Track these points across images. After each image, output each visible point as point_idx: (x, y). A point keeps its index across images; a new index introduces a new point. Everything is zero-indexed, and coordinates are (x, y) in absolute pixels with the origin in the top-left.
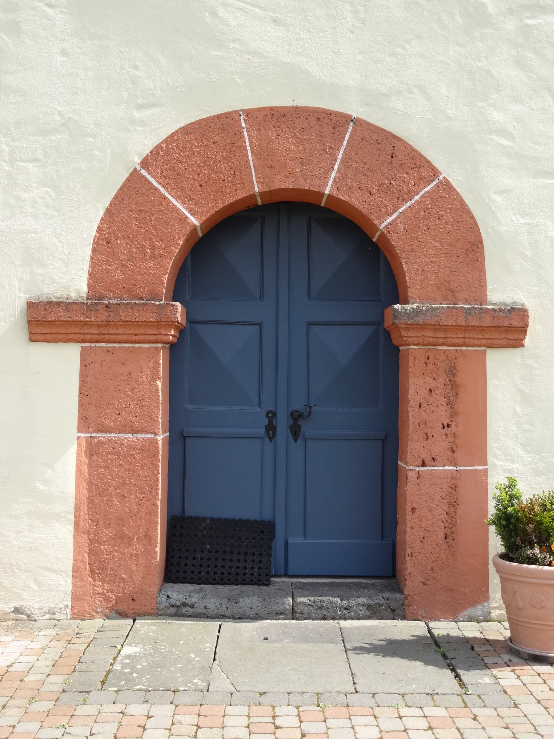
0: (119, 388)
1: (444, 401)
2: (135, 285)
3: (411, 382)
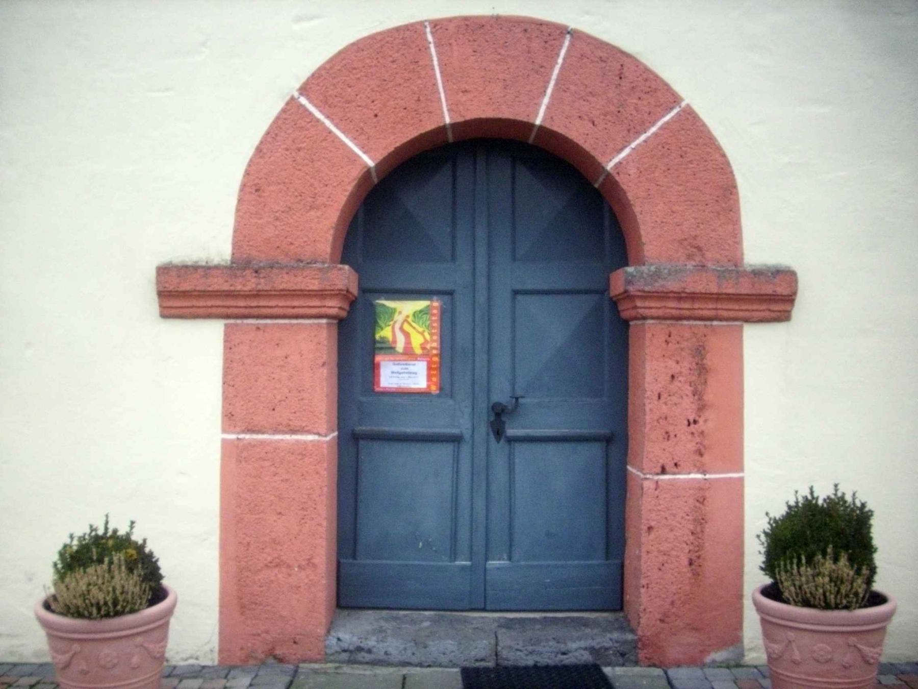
0: (273, 376)
1: (688, 389)
2: (292, 244)
3: (648, 366)
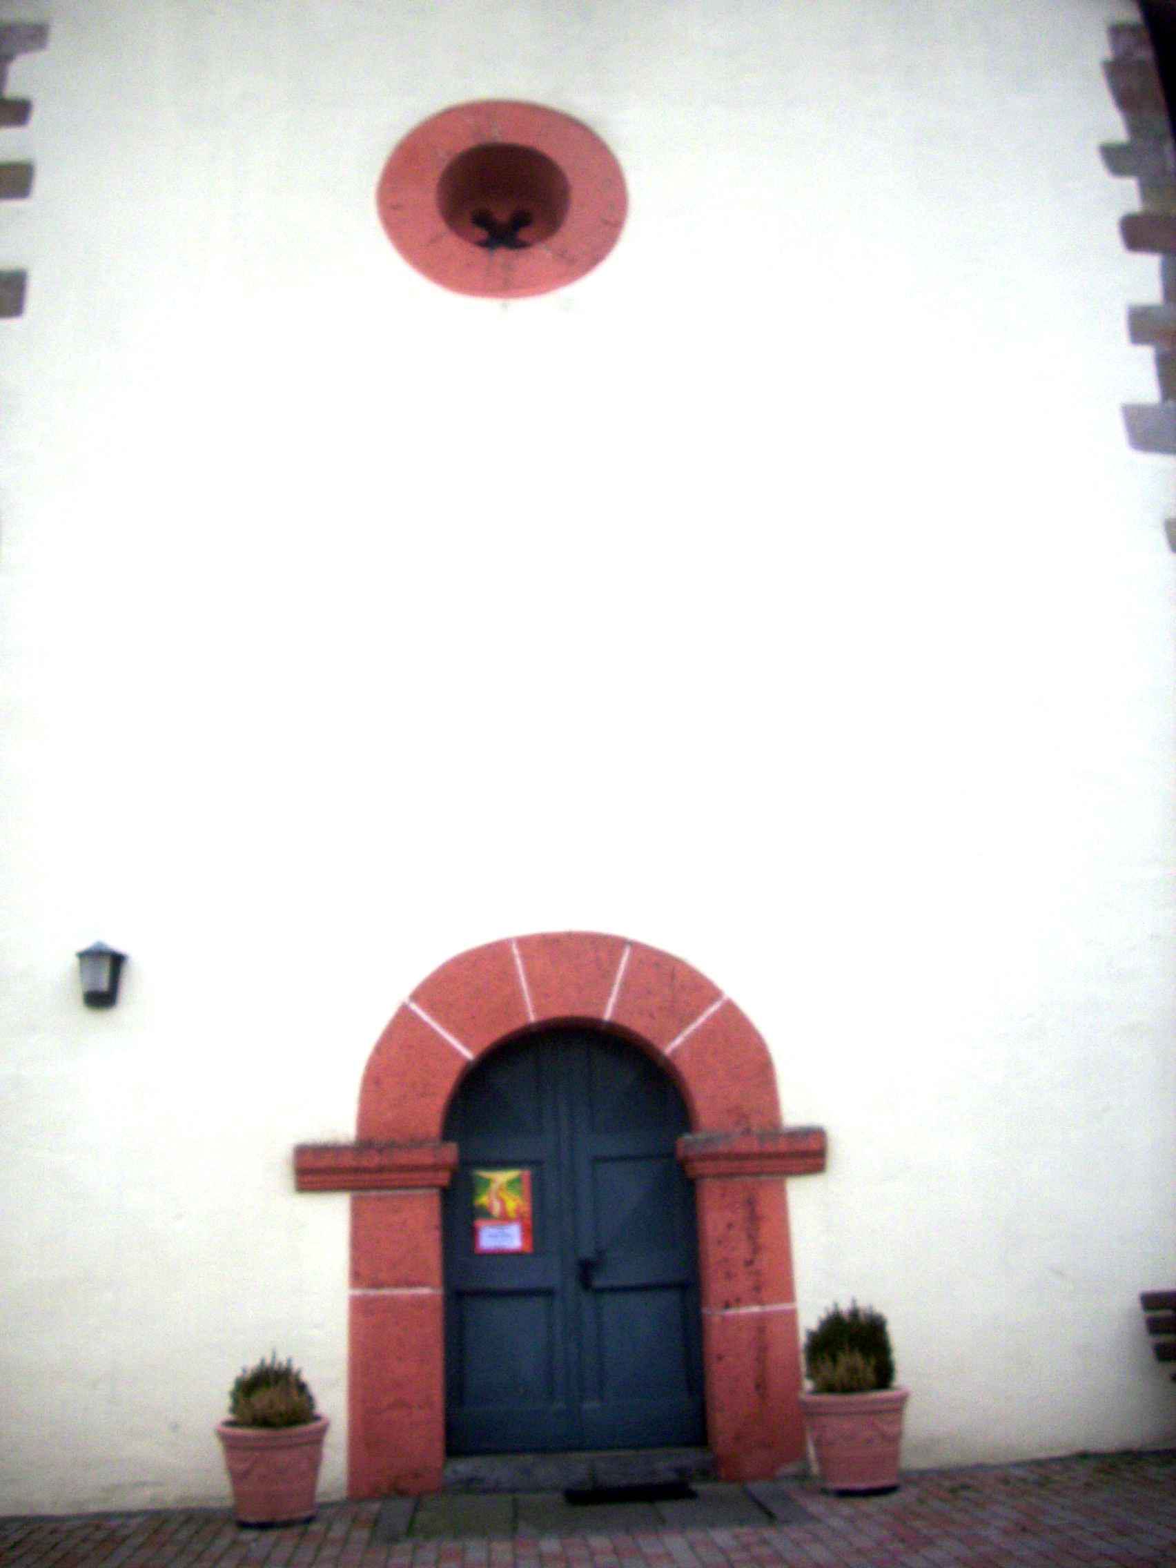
1: (743, 1236)
